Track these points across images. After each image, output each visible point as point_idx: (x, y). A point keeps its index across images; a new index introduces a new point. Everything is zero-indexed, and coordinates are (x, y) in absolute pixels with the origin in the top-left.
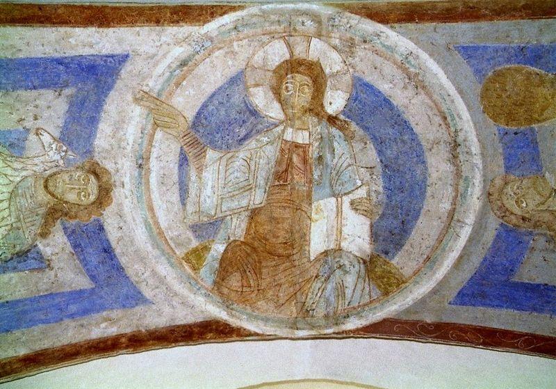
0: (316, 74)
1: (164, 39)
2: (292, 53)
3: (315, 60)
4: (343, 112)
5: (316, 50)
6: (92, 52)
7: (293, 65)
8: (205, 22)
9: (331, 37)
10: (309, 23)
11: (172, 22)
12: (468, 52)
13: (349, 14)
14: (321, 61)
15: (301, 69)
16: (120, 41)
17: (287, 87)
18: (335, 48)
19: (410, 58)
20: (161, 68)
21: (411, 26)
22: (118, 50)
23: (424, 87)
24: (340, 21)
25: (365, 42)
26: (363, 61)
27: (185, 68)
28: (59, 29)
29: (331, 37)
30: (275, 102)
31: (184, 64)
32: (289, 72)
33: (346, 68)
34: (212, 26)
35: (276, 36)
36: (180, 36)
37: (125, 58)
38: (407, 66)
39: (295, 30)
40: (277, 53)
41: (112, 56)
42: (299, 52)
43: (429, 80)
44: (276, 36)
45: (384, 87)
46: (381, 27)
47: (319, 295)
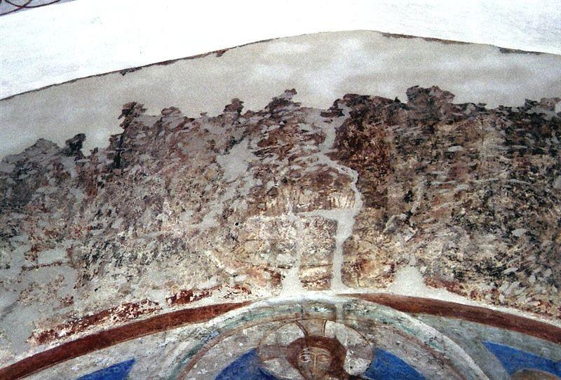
0: (335, 348)
1: (168, 339)
2: (306, 333)
3: (332, 337)
4: (366, 373)
5: (331, 328)
6: (96, 369)
7: (309, 341)
8: (210, 318)
9: (347, 319)
10: (322, 310)
11: (175, 325)
12: (498, 351)
13: (366, 302)
14: (338, 337)
15: (319, 343)
16: (123, 352)
17: (304, 358)
18: (353, 327)
19: (434, 341)
20: (169, 361)
21: (436, 318)
22: (124, 359)
23: (451, 365)
24: (356, 306)
25: (386, 323)
26: (384, 340)
27: (194, 356)
28: (60, 365)
29: (347, 319)
30: (292, 369)
31: (191, 353)
32: (305, 346)
33: (366, 342)
34: (218, 321)
35: (287, 321)
36: (185, 333)
37: (132, 362)
38: (431, 346)
39: (308, 315)
40: (292, 333)
41: (118, 365)
42: (313, 330)
43: (459, 363)
44: (287, 321)
45: (409, 360)
46: (404, 315)
47: (348, 205)
